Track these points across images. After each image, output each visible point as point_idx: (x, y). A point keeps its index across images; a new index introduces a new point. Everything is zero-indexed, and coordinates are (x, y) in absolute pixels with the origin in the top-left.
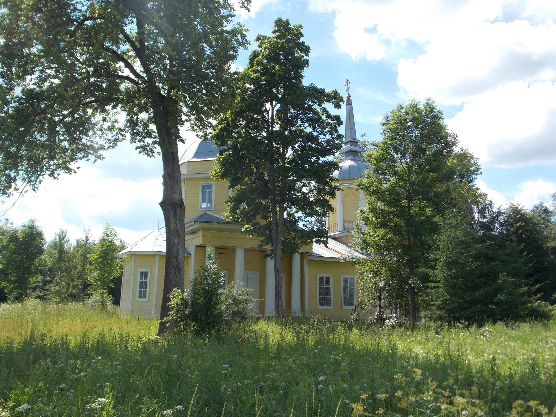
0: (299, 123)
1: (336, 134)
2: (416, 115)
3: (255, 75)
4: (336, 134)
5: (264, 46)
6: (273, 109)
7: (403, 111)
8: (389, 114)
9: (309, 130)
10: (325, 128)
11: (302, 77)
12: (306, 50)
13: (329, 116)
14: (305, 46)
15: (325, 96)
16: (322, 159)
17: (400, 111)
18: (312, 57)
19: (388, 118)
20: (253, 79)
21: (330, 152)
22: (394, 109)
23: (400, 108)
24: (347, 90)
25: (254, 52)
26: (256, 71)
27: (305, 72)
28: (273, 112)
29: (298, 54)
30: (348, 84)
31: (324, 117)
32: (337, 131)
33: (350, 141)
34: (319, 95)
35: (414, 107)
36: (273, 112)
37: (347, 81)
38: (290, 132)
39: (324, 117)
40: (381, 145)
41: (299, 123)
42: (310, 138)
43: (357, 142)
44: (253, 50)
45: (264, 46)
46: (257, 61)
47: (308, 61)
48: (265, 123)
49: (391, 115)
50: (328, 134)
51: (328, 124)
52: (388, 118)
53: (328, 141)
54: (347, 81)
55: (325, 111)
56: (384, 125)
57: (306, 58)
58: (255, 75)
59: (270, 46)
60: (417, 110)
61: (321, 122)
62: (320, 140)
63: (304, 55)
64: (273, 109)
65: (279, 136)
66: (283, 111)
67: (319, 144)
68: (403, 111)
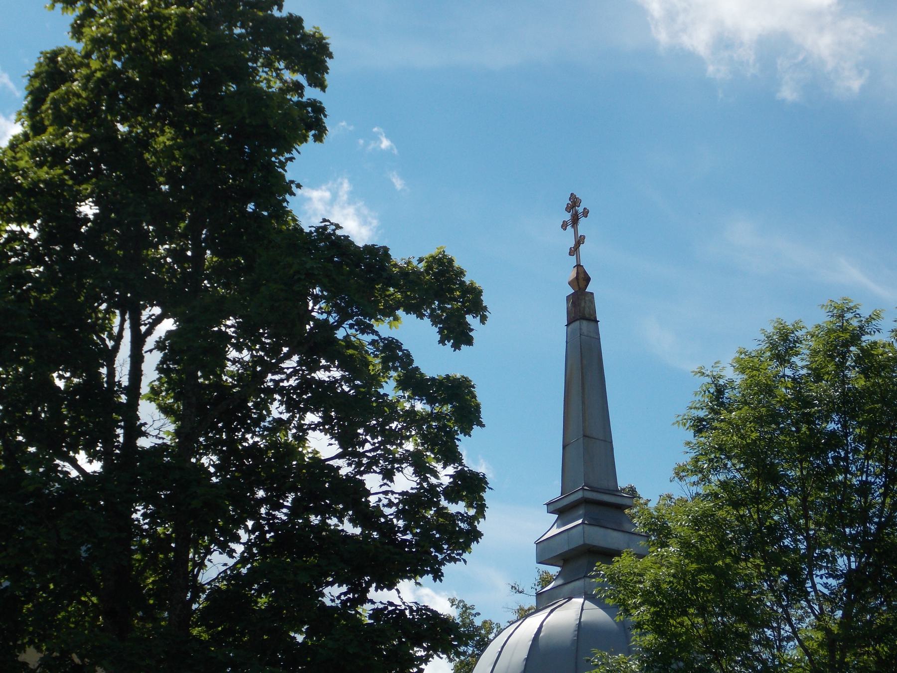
0: (277, 410)
1: (451, 470)
2: (856, 380)
3: (44, 173)
4: (451, 470)
5: (92, 30)
6: (138, 341)
7: (801, 362)
8: (730, 374)
9: (322, 445)
10: (396, 437)
11: (287, 188)
12: (312, 56)
13: (413, 382)
14: (305, 37)
15: (391, 281)
16: (379, 596)
17: (782, 359)
18: (334, 96)
19: (720, 391)
20: (33, 191)
21: (422, 562)
22: (752, 347)
23: (783, 345)
24: (574, 251)
25: (52, 57)
26: (56, 156)
27: (302, 163)
28: (137, 359)
29: (274, 77)
30: (575, 220)
31: (389, 388)
32: (451, 456)
33: (585, 502)
34: (363, 277)
35: (846, 344)
36: (137, 359)
37: (574, 202)
38: (231, 453)
39: (389, 388)
40: (680, 526)
41: (277, 410)
42: (325, 488)
43: (620, 508)
44: (50, 47)
45: (92, 30)
46: (55, 102)
47: (318, 108)
48: (102, 411)
49: (739, 379)
50: (409, 470)
51: (411, 417)
52: (720, 391)
53: (412, 504)
54: (574, 202)
55: (392, 351)
56: (700, 426)
57: (311, 93)
58: (44, 173)
59: (119, 30)
60: (867, 354)
61: (379, 412)
62: (373, 500)
63: (301, 79)
64: (138, 341)
65: (161, 475)
66: (191, 354)
67: (367, 516)
68: (801, 362)
